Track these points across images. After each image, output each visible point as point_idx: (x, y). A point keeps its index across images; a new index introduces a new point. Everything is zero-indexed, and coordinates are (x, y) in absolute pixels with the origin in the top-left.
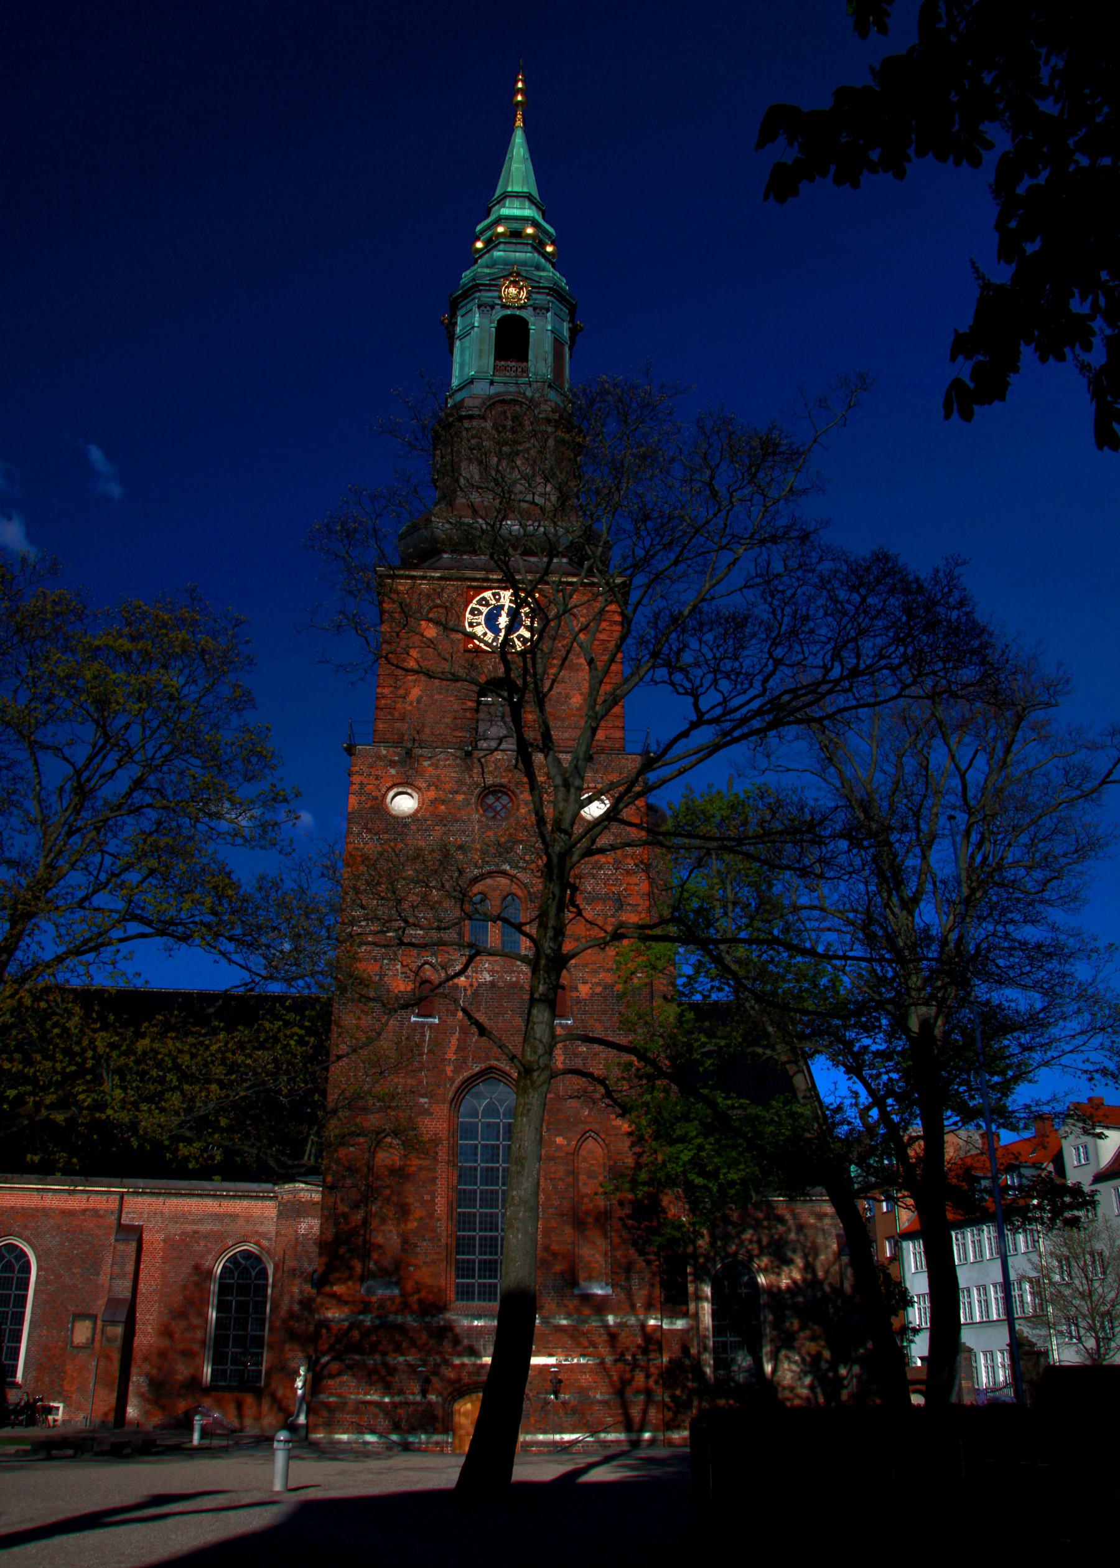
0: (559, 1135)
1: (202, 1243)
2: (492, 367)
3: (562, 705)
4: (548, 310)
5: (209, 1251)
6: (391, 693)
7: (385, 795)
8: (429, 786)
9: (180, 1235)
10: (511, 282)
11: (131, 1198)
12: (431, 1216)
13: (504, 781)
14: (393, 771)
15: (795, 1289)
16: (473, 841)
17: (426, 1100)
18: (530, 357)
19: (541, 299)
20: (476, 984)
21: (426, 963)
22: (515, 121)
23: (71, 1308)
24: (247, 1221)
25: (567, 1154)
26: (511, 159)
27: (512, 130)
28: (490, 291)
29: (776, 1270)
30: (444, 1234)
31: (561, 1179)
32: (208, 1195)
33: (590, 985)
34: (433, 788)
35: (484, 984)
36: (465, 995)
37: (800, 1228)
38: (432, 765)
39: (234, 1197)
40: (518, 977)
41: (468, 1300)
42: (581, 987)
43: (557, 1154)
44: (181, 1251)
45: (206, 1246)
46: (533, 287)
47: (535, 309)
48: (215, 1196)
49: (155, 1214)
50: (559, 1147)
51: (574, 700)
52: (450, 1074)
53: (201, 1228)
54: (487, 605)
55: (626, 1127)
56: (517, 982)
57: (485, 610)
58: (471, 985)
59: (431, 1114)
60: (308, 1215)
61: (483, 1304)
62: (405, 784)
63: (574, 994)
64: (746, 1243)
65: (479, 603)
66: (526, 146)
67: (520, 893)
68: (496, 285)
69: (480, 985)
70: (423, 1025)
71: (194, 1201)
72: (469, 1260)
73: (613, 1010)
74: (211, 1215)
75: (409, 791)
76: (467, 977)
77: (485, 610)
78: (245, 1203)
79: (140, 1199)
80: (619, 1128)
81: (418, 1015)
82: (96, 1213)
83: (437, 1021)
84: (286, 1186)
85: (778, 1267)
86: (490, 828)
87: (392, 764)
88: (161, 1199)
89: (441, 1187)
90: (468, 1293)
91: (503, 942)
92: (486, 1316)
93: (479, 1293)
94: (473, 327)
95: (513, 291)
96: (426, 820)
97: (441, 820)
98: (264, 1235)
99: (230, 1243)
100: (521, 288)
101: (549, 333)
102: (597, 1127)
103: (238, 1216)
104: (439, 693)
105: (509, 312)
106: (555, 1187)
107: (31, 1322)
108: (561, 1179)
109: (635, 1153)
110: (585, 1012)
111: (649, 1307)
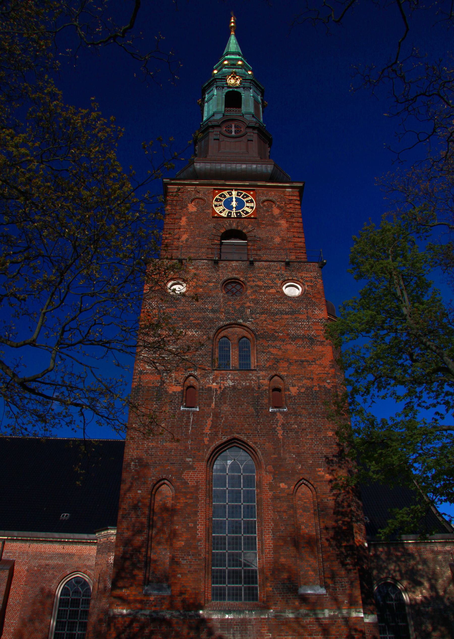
0: (281, 482)
3: (269, 242)
4: (250, 89)
5: (54, 578)
9: (37, 567)
10: (232, 77)
11: (9, 543)
12: (194, 537)
15: (426, 601)
16: (220, 307)
17: (190, 459)
19: (247, 84)
20: (223, 387)
21: (191, 375)
22: (231, 20)
24: (80, 558)
25: (288, 494)
26: (229, 44)
27: (229, 35)
28: (222, 81)
29: (413, 590)
30: (203, 551)
31: (285, 512)
32: (56, 541)
33: (297, 387)
35: (229, 387)
36: (216, 394)
37: (425, 562)
38: (194, 268)
39: (72, 542)
40: (250, 383)
41: (221, 599)
42: (291, 388)
43: (281, 495)
44: (37, 577)
45: (53, 574)
47: (244, 88)
48: (60, 542)
50: (283, 490)
51: (276, 240)
52: (206, 443)
53: (51, 562)
54: (225, 197)
55: (328, 477)
56: (250, 386)
57: (224, 199)
58: (220, 388)
59: (194, 468)
61: (231, 602)
63: (287, 393)
64: (392, 572)
66: (236, 40)
67: (249, 336)
68: (224, 79)
69: (225, 388)
70: (189, 412)
71: (48, 545)
72: (221, 570)
73: (313, 402)
74: (58, 554)
76: (217, 383)
77: (224, 199)
78: (79, 546)
79: (15, 544)
80: (323, 476)
81: (185, 407)
83: (198, 409)
84: (103, 533)
85: (413, 587)
86: (230, 300)
88: (28, 544)
89: (201, 516)
90: (221, 595)
91: (240, 364)
92: (234, 611)
93: (229, 595)
94: (214, 95)
95: (233, 81)
98: (89, 567)
99: (68, 572)
100: (237, 79)
101: (252, 97)
102: (307, 476)
103: (74, 555)
104: (199, 237)
105: (231, 90)
108: (285, 512)
109: (334, 495)
110: (295, 404)
111: (352, 604)
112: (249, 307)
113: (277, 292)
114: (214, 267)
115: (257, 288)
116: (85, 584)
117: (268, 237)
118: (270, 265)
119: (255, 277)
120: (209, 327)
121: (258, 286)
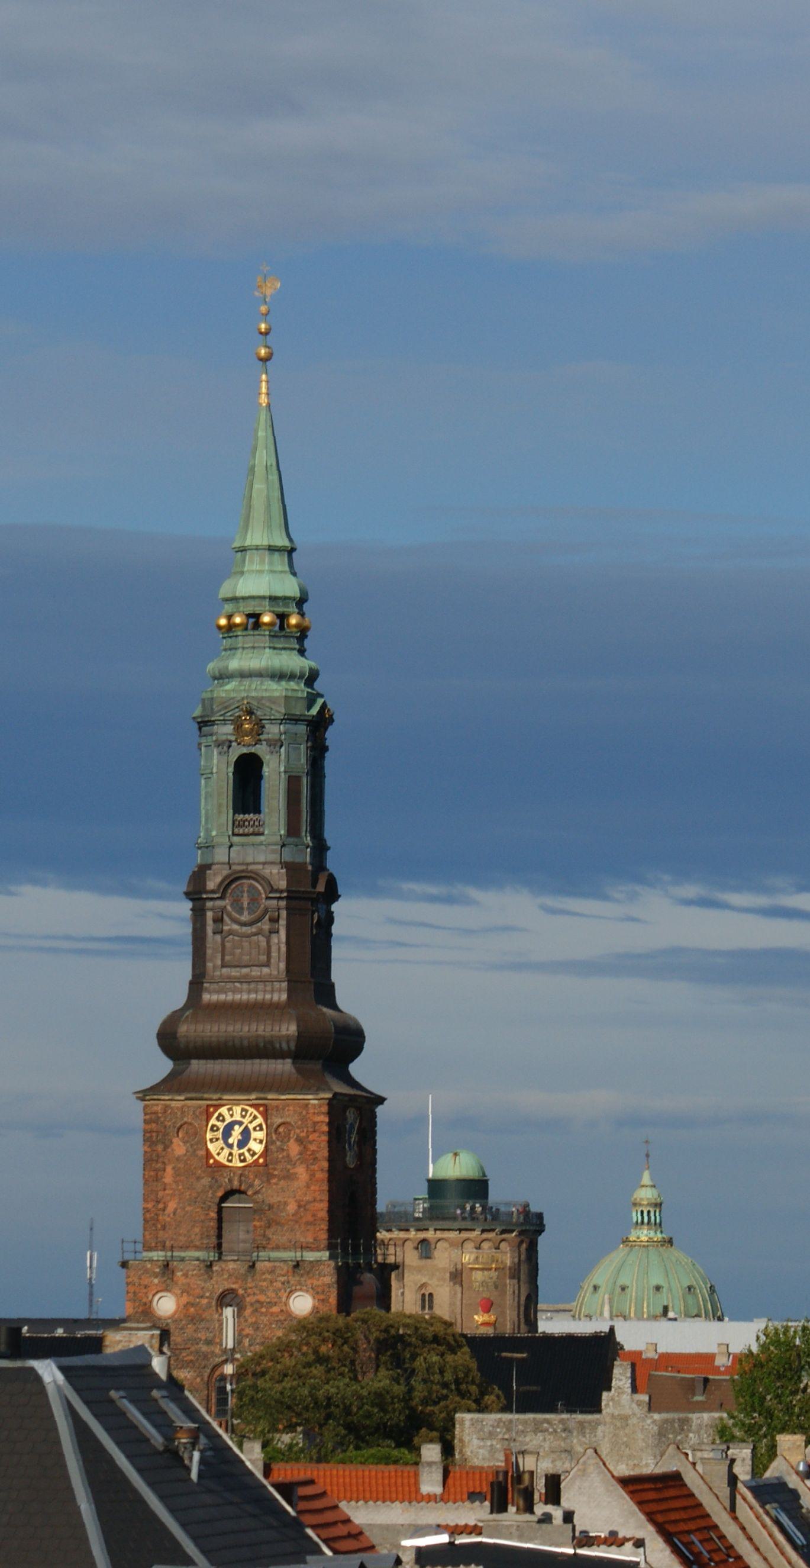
3: (282, 1212)
7: (151, 1302)
8: (182, 1293)
13: (234, 1286)
14: (156, 1281)
34: (185, 1294)
65: (218, 1119)
87: (156, 1276)
95: (286, 1438)
96: (181, 1320)
97: (192, 1320)
104: (190, 1205)
112: (247, 1336)
113: (282, 1311)
114: (207, 1273)
115: (258, 1305)
116: (305, 684)
117: (280, 1202)
118: (275, 1267)
119: (256, 1287)
120: (203, 1365)
121: (258, 1301)
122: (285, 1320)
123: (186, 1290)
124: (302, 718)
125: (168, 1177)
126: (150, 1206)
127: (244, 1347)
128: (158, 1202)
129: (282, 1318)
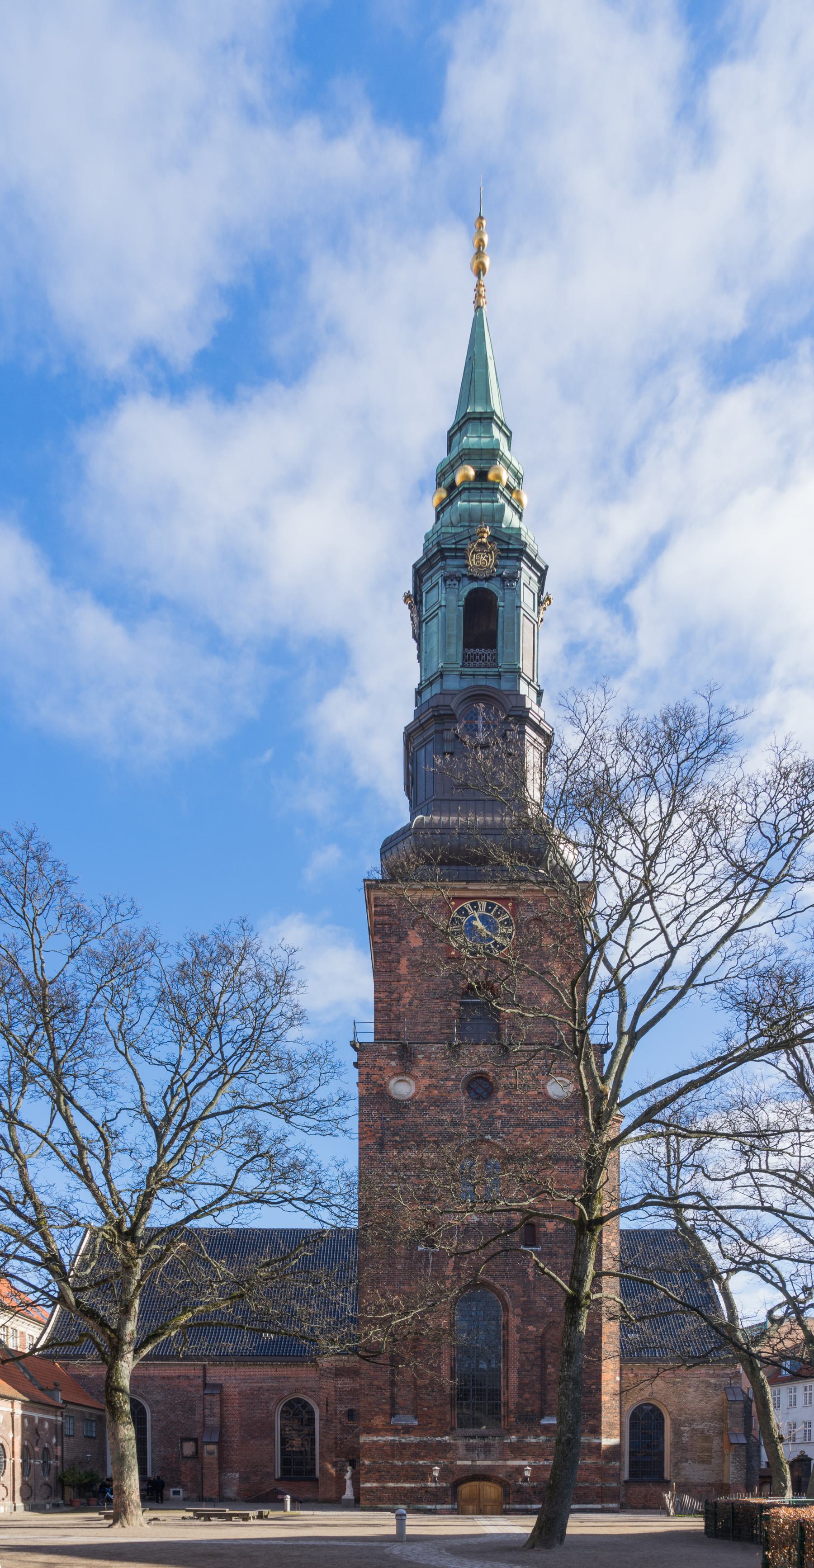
1: (266, 1394)
2: (460, 656)
5: (271, 1399)
6: (387, 997)
14: (393, 1063)
18: (500, 643)
23: (179, 1435)
38: (425, 1057)
46: (502, 550)
49: (230, 1377)
50: (531, 1332)
60: (343, 1376)
62: (404, 1072)
63: (542, 1229)
75: (407, 1079)
82: (187, 1378)
87: (391, 1057)
96: (422, 1102)
97: (435, 1102)
106: (527, 1358)
107: (152, 1443)
110: (551, 1242)
112: (500, 1117)
122: (543, 1103)
123: (429, 1072)
124: (485, 416)
125: (403, 968)
126: (382, 995)
127: (496, 1128)
128: (391, 993)
129: (539, 1100)
